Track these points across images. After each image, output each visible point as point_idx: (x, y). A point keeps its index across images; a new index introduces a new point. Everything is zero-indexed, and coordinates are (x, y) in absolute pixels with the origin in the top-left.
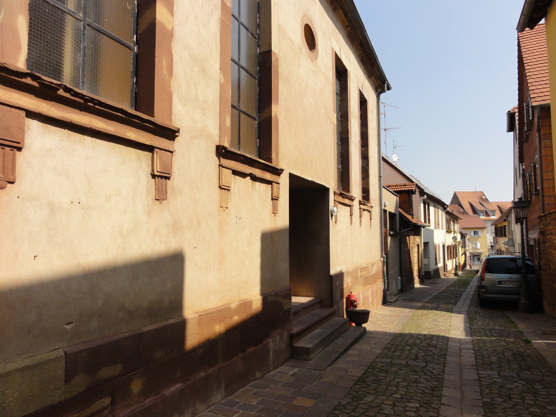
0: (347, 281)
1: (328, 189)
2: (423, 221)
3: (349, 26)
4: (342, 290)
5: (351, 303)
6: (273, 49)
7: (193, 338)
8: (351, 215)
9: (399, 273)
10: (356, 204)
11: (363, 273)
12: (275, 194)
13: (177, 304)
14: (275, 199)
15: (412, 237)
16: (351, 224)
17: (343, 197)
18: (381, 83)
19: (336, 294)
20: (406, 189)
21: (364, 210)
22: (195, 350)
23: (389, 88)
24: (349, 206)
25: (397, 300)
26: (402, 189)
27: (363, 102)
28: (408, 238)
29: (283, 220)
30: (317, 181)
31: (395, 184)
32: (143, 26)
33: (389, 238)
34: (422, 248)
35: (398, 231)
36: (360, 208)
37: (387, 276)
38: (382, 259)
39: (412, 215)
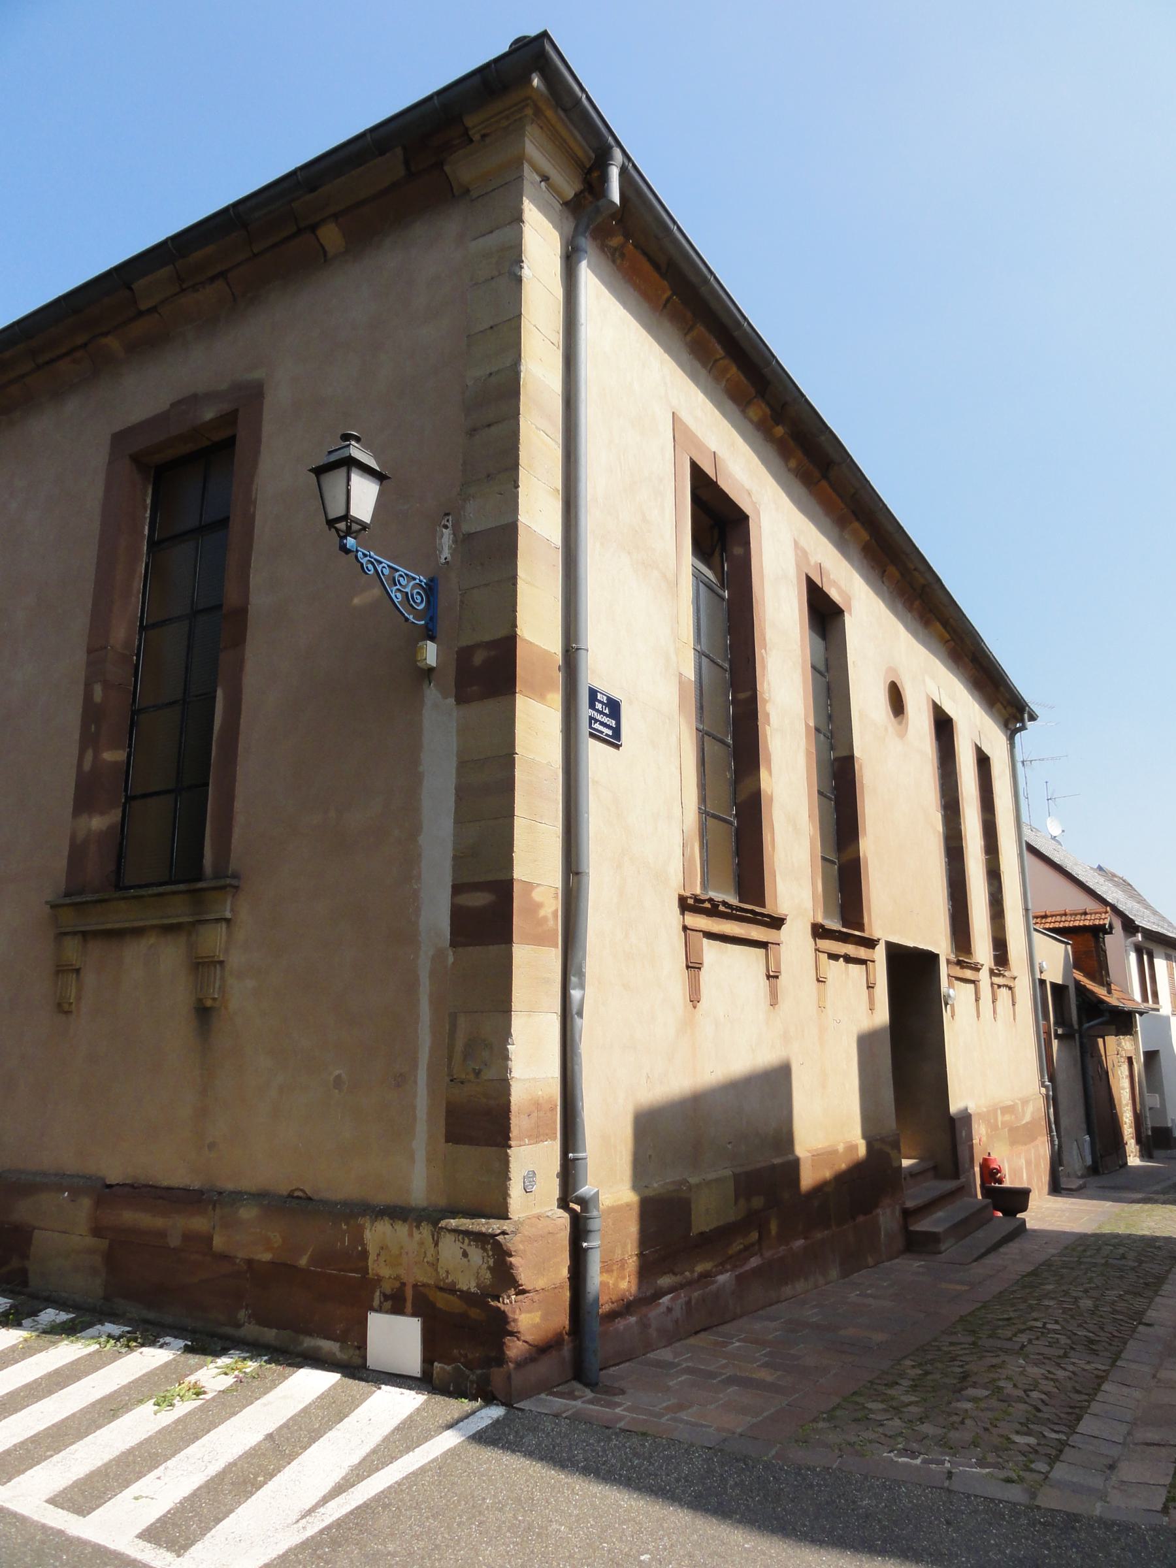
0: (980, 1132)
1: (937, 956)
2: (1137, 996)
3: (953, 639)
4: (971, 1147)
5: (990, 1173)
6: (857, 753)
7: (808, 1178)
8: (977, 1000)
9: (1084, 1126)
10: (984, 976)
11: (1007, 1118)
12: (871, 980)
13: (784, 1138)
14: (870, 987)
15: (1111, 1040)
16: (978, 1016)
17: (962, 967)
18: (1015, 711)
19: (962, 1150)
20: (1087, 923)
21: (999, 986)
22: (819, 1189)
23: (1033, 718)
24: (973, 982)
25: (1080, 1188)
26: (1077, 924)
27: (983, 762)
28: (1100, 1041)
29: (882, 1016)
30: (921, 946)
31: (1059, 909)
32: (742, 797)
33: (1055, 1043)
34: (1138, 1066)
35: (1076, 1027)
36: (992, 984)
37: (1056, 1127)
38: (1043, 1090)
39: (1108, 986)
